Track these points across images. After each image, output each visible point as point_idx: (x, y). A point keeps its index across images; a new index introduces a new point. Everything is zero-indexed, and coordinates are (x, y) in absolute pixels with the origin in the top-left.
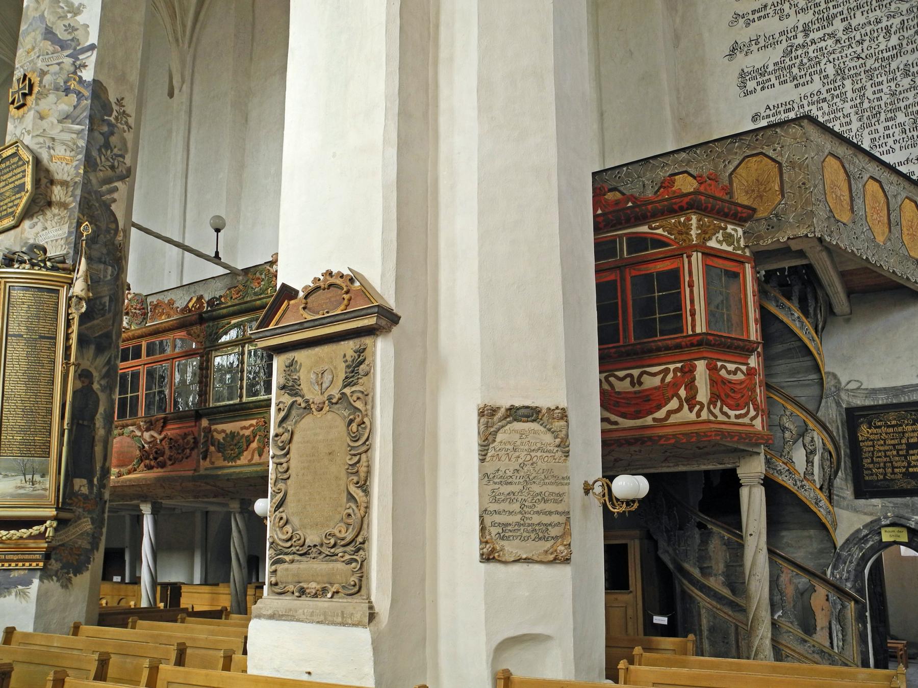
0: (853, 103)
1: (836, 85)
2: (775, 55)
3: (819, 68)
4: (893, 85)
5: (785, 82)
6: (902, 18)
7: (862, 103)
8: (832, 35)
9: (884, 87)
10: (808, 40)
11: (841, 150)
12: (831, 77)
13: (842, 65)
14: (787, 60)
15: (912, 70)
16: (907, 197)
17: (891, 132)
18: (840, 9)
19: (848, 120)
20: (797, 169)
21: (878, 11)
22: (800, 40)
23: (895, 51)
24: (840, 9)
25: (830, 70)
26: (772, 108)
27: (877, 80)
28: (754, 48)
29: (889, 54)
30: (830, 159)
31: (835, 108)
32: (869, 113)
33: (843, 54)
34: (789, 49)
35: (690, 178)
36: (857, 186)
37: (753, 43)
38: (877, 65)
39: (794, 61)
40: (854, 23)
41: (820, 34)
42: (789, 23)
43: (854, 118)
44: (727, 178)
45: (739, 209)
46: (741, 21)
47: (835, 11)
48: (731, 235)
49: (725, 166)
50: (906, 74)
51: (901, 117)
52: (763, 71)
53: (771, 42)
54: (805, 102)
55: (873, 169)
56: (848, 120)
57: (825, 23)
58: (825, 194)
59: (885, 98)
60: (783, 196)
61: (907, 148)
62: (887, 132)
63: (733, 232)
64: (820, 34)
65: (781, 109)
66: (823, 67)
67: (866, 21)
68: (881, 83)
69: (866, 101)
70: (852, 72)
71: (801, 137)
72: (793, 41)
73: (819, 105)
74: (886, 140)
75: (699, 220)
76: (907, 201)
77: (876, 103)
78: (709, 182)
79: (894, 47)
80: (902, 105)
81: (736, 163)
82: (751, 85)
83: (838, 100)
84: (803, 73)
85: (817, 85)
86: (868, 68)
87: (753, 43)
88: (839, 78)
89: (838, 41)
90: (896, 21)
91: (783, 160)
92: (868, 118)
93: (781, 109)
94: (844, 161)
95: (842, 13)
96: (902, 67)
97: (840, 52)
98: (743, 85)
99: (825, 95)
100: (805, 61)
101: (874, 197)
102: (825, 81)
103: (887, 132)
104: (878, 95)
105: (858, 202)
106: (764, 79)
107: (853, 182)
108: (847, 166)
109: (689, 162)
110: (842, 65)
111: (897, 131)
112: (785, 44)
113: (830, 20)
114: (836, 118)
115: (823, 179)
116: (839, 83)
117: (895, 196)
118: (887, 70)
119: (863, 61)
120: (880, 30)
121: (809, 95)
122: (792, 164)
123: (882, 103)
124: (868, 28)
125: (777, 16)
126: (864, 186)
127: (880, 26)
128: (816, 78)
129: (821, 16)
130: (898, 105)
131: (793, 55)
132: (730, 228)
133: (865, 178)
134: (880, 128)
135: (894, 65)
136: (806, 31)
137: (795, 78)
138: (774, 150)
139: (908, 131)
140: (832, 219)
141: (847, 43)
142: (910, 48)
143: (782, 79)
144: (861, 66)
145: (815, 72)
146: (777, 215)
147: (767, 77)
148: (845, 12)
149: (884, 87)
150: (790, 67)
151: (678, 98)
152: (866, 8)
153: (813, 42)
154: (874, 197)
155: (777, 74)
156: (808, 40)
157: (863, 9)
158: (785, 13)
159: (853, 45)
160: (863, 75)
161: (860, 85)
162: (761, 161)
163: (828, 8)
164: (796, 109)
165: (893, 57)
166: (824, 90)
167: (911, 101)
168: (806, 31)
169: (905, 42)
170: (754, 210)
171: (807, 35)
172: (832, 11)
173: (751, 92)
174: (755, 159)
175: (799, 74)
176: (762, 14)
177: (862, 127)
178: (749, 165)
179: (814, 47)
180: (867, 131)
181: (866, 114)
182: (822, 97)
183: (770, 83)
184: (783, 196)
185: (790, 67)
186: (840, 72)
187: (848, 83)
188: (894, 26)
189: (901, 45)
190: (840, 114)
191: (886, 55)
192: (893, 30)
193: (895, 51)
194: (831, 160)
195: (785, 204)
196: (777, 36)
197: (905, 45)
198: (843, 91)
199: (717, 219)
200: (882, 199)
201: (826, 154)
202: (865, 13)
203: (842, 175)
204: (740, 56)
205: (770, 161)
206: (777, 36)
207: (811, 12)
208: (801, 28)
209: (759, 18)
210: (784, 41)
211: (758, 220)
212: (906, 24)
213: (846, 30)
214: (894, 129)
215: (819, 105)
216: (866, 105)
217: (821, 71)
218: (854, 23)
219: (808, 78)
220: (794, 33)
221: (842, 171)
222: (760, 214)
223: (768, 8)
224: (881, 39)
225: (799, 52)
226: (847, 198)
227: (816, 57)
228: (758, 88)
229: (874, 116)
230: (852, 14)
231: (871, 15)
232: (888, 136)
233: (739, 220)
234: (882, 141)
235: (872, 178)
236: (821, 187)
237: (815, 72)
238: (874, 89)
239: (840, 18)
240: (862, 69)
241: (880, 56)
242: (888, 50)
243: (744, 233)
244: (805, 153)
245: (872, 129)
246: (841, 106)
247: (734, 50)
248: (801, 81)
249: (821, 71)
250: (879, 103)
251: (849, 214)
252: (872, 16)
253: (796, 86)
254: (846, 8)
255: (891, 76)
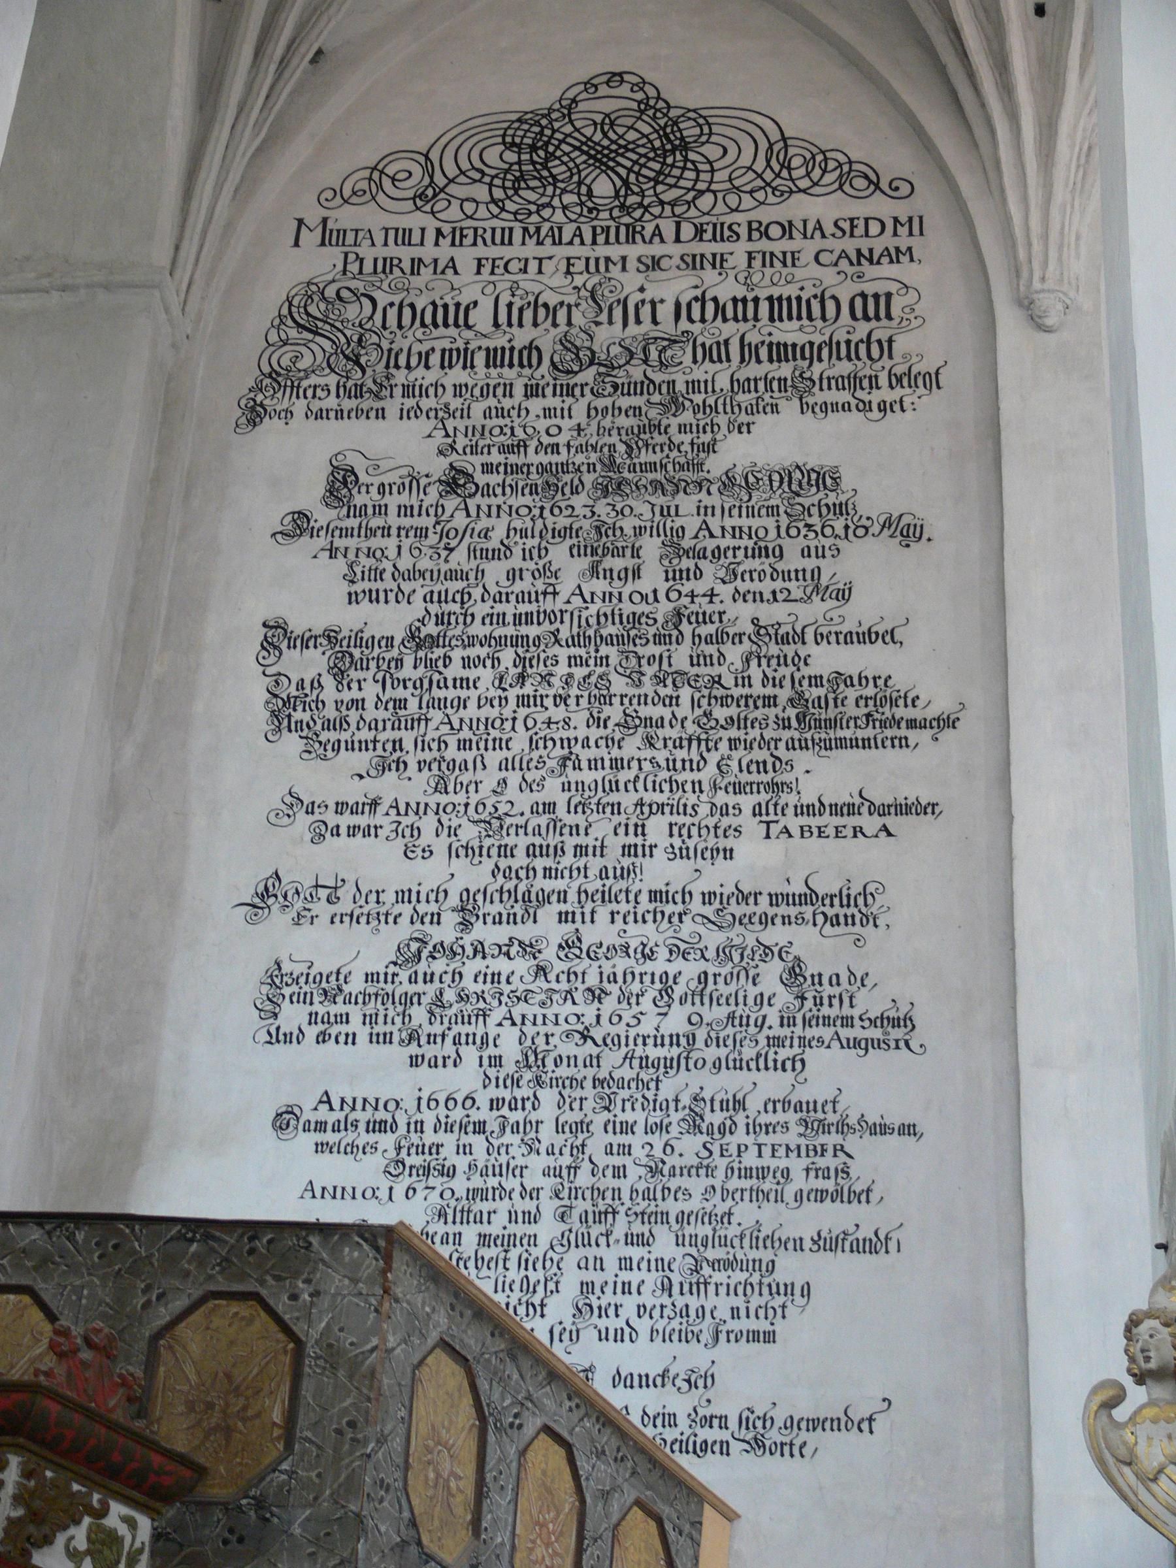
0: (550, 1161)
1: (519, 1093)
2: (369, 952)
3: (480, 1032)
4: (658, 1141)
5: (387, 1038)
6: (702, 966)
7: (574, 1169)
8: (529, 949)
9: (636, 1141)
10: (467, 940)
11: (472, 1340)
12: (509, 1068)
13: (540, 1041)
14: (404, 976)
15: (709, 1117)
16: (638, 1503)
17: (634, 1277)
18: (560, 884)
19: (530, 1205)
20: (341, 1374)
21: (650, 925)
22: (446, 932)
23: (675, 1051)
24: (560, 884)
25: (509, 1046)
26: (336, 1104)
27: (622, 1117)
28: (322, 909)
29: (661, 1052)
30: (440, 1355)
31: (503, 1159)
32: (587, 1205)
33: (462, 1162)
34: (414, 946)
35: (37, 1315)
36: (502, 1450)
37: (323, 893)
38: (627, 1073)
39: (420, 987)
40: (590, 936)
41: (501, 934)
42: (429, 873)
43: (548, 1206)
44: (143, 1345)
45: (157, 1460)
46: (303, 820)
47: (549, 885)
48: (113, 1539)
49: (147, 1305)
50: (694, 1124)
51: (664, 1245)
52: (331, 987)
53: (369, 911)
54: (429, 1117)
55: (554, 1407)
56: (530, 1205)
57: (519, 909)
58: (407, 1467)
59: (633, 1172)
60: (289, 1446)
61: (667, 1338)
62: (625, 1276)
63: (123, 1530)
64: (501, 934)
65: (362, 1116)
66: (493, 1031)
67: (618, 942)
68: (628, 1128)
69: (586, 1166)
70: (563, 1071)
71: (370, 1281)
72: (427, 928)
73: (465, 1139)
74: (619, 1298)
75: (27, 1474)
76: (637, 1513)
77: (609, 1182)
78: (86, 1355)
79: (675, 1040)
80: (673, 1207)
81: (179, 1304)
82: (292, 1016)
83: (515, 1139)
84: (437, 1029)
85: (465, 1077)
86: (603, 1074)
87: (323, 893)
88: (528, 1075)
89: (541, 971)
90: (690, 969)
91: (312, 1333)
92: (584, 1219)
93: (362, 1116)
94: (478, 1369)
95: (563, 897)
96: (685, 1100)
97: (543, 1004)
98: (270, 1009)
99: (482, 1113)
100: (450, 995)
101: (547, 1490)
102: (492, 1073)
103: (625, 1276)
104: (617, 1161)
105: (498, 1501)
106: (334, 1009)
107: (491, 1438)
108: (483, 1385)
109: (44, 1262)
110: (540, 1041)
111: (652, 1279)
112: (404, 930)
113: (532, 903)
114: (502, 1193)
115: (408, 1421)
116: (525, 1092)
117: (605, 1495)
118: (650, 1095)
119: (595, 1051)
120: (647, 979)
121: (442, 1099)
122: (332, 1354)
123: (625, 1185)
124: (621, 964)
125: (400, 842)
126: (523, 1453)
127: (649, 967)
128: (470, 1054)
129: (510, 885)
130: (663, 1206)
131: (422, 967)
132: (117, 1509)
133: (530, 1429)
134: (610, 1259)
135: (667, 1089)
136: (467, 913)
137: (413, 1037)
138: (294, 1297)
139: (676, 1289)
140: (413, 1550)
141: (564, 986)
142: (712, 1053)
143: (380, 1028)
144: (594, 1061)
145: (470, 1039)
146: (260, 1504)
147: (339, 1008)
148: (572, 896)
149: (636, 1141)
150: (409, 1000)
151: (76, 983)
152: (623, 907)
153: (479, 950)
154: (547, 1490)
155: (370, 1009)
156: (467, 940)
157: (614, 906)
158: (423, 842)
159: (578, 996)
160: (589, 1091)
161: (576, 1116)
162: (250, 1321)
163: (531, 870)
164: (402, 1129)
165: (669, 1064)
166: (483, 1099)
167: (695, 1204)
168: (467, 913)
169: (701, 1035)
170: (201, 1471)
171: (466, 925)
172: (540, 883)
173: (288, 1038)
174: (235, 1307)
175: (427, 1029)
176: (362, 820)
177: (565, 1241)
178: (217, 1322)
179: (478, 964)
180: (574, 1256)
181: (581, 1206)
182: (476, 1116)
183: (344, 1028)
184: (289, 1446)
185: (409, 1000)
186: (532, 1058)
187: (548, 1096)
188: (682, 980)
189: (691, 1039)
190: (511, 1183)
191: (653, 1053)
192: (679, 990)
193: (675, 1051)
194: (442, 1363)
195: (291, 1474)
196: (389, 897)
197: (700, 1043)
198: (533, 1117)
199: (82, 1479)
200: (569, 1502)
201: (430, 1342)
202: (619, 918)
203: (466, 1413)
204: (278, 919)
205: (273, 1327)
206: (389, 897)
207: (488, 865)
208: (454, 900)
209: (352, 831)
210: (404, 920)
211: (205, 1506)
212: (711, 986)
213: (565, 946)
214: (644, 1274)
215: (465, 1139)
216: (584, 1179)
217: (485, 1041)
218: (590, 936)
219: (449, 1049)
220: (433, 907)
221: (468, 1400)
222: (215, 1490)
223: (381, 810)
224: (646, 1003)
225: (439, 966)
226: (468, 1486)
227: (480, 997)
228: (312, 1032)
229: (601, 1216)
230: (587, 910)
231: (632, 929)
232: (626, 1288)
233: (147, 1491)
234: (608, 1298)
235: (547, 1430)
236: (397, 1444)
237: (470, 1039)
238: (610, 1138)
239: (556, 907)
240: (590, 1072)
241: (639, 1052)
242: (659, 1042)
243: (157, 1536)
244: (376, 1330)
245: (591, 1252)
246: (520, 1161)
247: (266, 895)
248: (430, 1051)
249: (485, 1041)
250: (616, 1183)
251: (465, 1535)
252: (636, 934)
253: (414, 1061)
254: (575, 886)
255: (657, 1116)
